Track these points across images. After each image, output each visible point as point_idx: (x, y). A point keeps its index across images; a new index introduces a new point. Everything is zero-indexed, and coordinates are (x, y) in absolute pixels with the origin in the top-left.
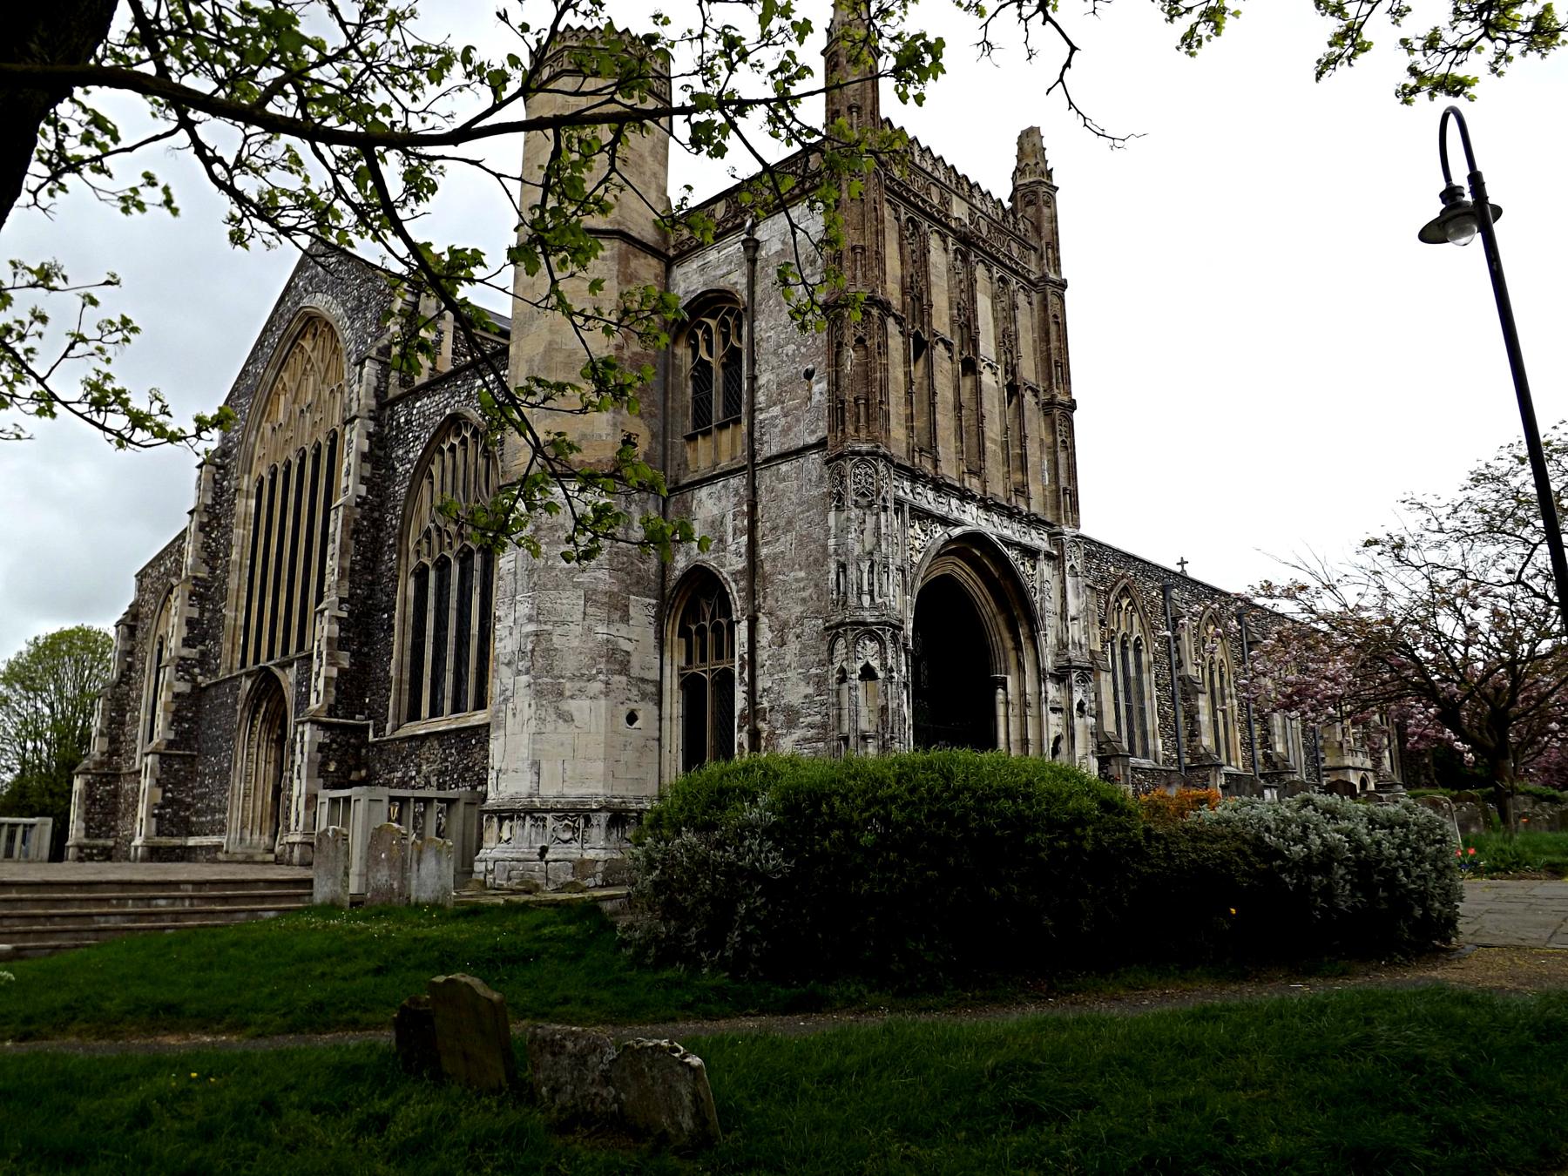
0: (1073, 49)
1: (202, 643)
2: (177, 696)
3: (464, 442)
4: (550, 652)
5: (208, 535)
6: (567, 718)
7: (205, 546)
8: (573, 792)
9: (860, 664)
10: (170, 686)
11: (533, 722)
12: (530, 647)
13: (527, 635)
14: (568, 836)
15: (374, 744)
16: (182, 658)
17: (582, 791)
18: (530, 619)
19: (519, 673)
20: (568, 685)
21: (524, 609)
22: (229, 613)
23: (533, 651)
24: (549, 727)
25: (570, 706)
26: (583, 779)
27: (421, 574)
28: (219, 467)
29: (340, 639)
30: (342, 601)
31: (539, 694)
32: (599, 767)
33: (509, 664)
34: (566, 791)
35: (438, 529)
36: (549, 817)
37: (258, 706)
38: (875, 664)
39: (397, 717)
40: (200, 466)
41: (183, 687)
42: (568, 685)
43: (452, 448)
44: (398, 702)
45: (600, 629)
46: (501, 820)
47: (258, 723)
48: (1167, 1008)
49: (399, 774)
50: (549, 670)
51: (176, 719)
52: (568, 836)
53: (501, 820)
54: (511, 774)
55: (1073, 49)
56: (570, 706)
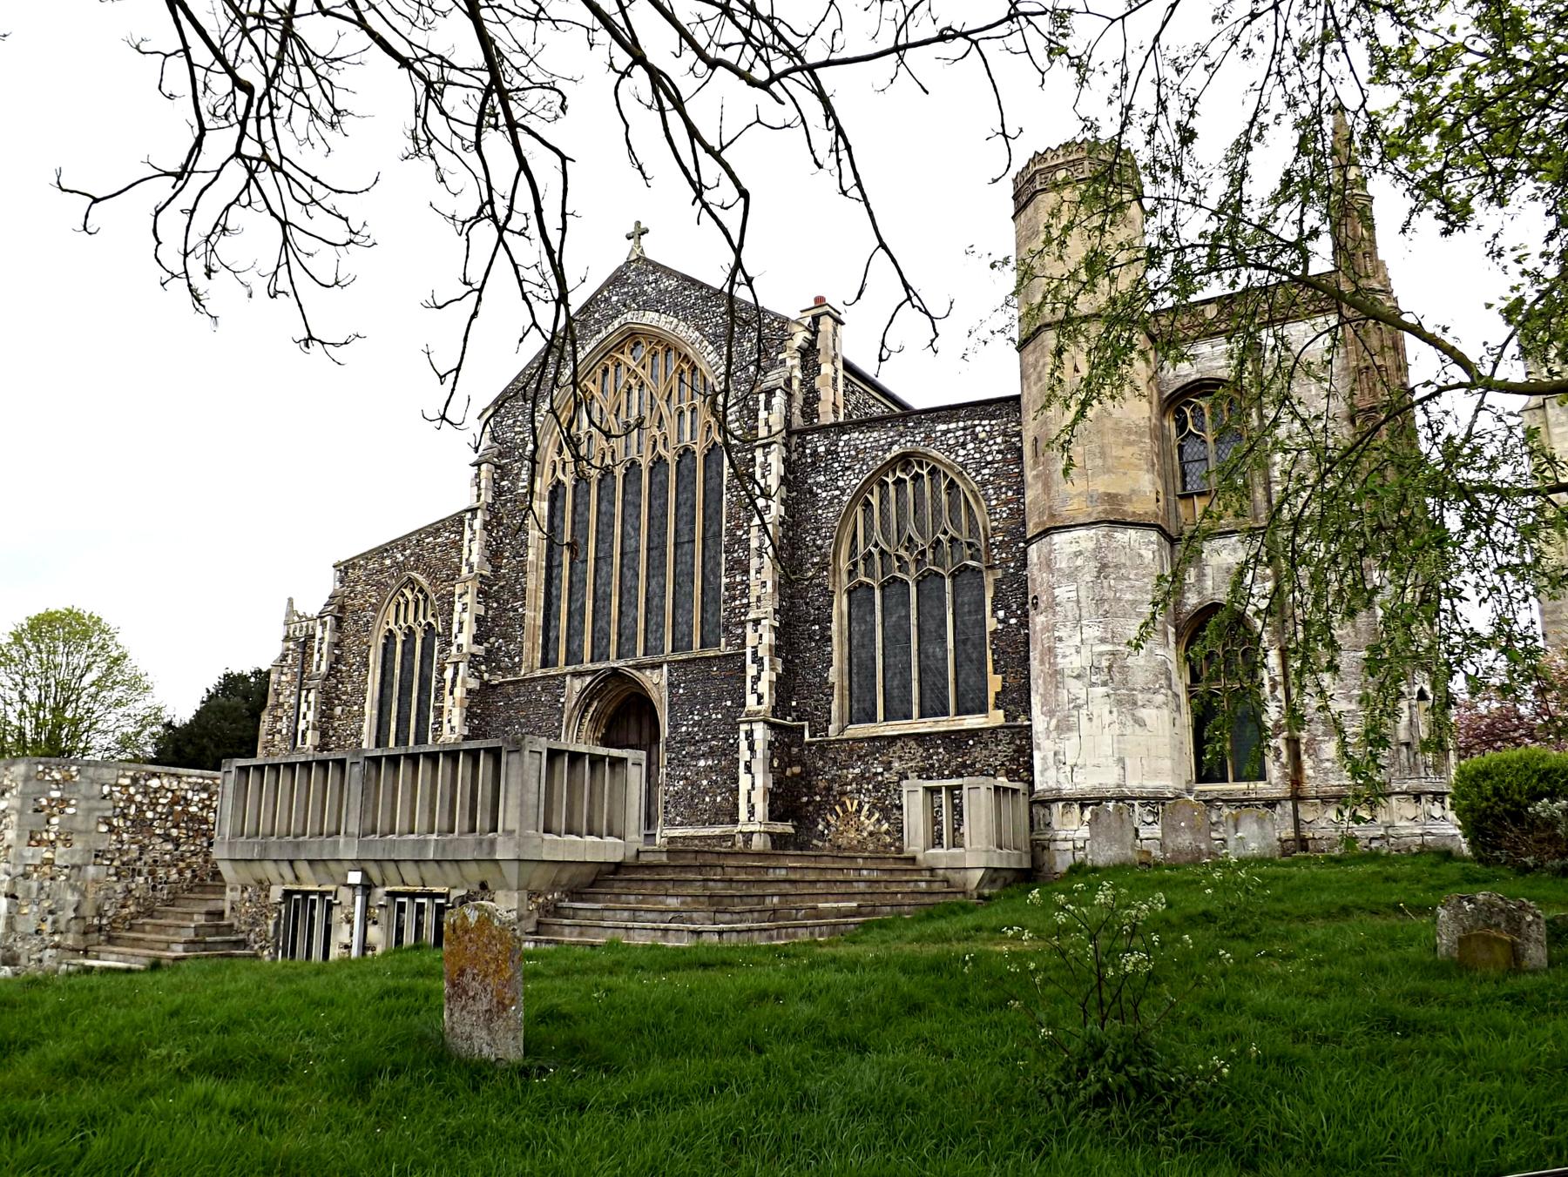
0: (564, 159)
1: (487, 640)
2: (469, 691)
3: (917, 478)
4: (1124, 669)
5: (490, 535)
6: (1141, 723)
7: (488, 545)
8: (1152, 784)
9: (1417, 689)
10: (464, 682)
11: (1116, 726)
12: (1105, 664)
13: (1101, 654)
14: (1150, 819)
15: (810, 744)
16: (473, 655)
17: (1157, 783)
18: (1103, 641)
19: (1093, 685)
20: (1140, 696)
21: (1093, 632)
22: (529, 614)
23: (1110, 668)
24: (1129, 731)
25: (1143, 713)
26: (1157, 773)
27: (861, 595)
28: (497, 467)
29: (777, 647)
30: (776, 611)
31: (1119, 703)
32: (1167, 764)
33: (1078, 677)
34: (1146, 783)
35: (882, 553)
36: (1136, 803)
37: (589, 705)
38: (1427, 688)
39: (841, 719)
40: (478, 464)
41: (474, 684)
42: (1140, 696)
43: (899, 482)
44: (841, 706)
45: (1158, 651)
46: (1083, 806)
47: (586, 721)
48: (839, 977)
49: (857, 771)
50: (1125, 682)
51: (469, 716)
52: (1150, 819)
53: (1083, 806)
54: (1089, 768)
55: (564, 159)
56: (1143, 713)
